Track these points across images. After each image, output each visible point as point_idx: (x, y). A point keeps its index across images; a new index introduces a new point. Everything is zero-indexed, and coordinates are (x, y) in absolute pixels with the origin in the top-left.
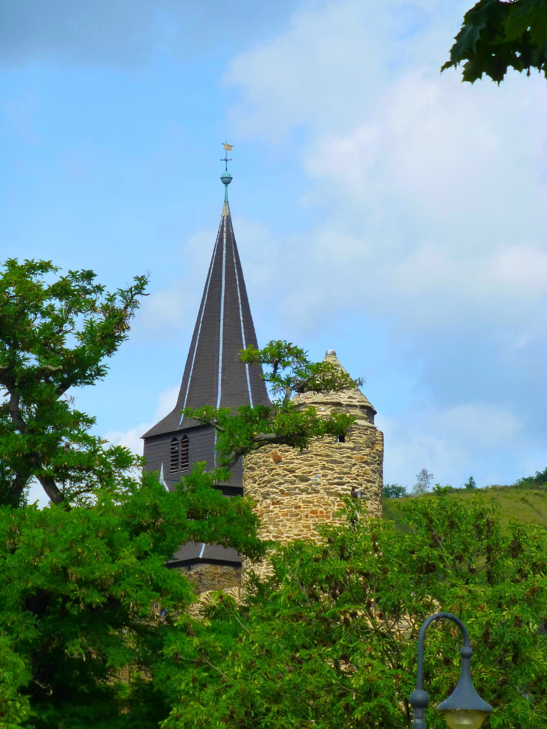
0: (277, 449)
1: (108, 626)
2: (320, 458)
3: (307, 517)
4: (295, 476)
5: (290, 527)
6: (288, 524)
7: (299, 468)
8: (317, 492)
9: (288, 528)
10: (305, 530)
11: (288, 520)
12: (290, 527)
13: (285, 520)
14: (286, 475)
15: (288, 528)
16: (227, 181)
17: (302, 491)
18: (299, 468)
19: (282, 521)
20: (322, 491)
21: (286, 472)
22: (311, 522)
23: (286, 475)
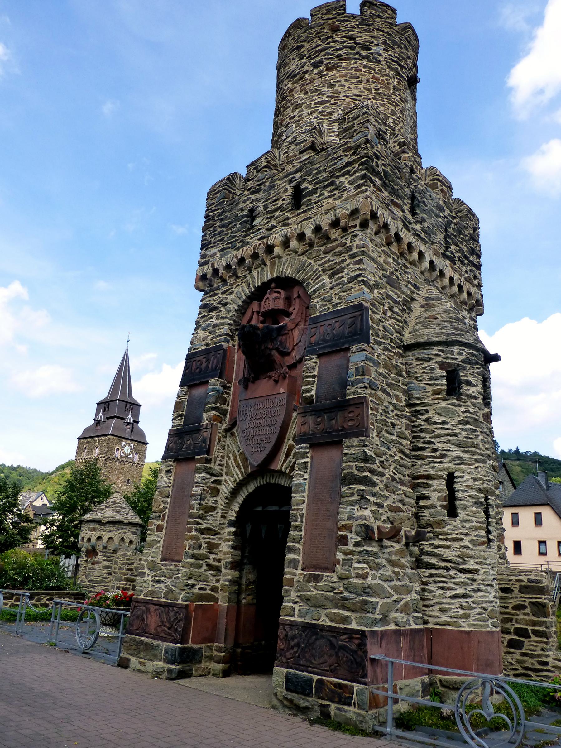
0: (334, 20)
1: (228, 665)
2: (382, 33)
3: (368, 81)
4: (355, 43)
5: (349, 87)
6: (347, 84)
7: (360, 37)
8: (379, 62)
9: (346, 88)
10: (366, 92)
11: (346, 81)
12: (349, 87)
13: (343, 81)
14: (344, 42)
15: (346, 88)
16: (128, 341)
17: (364, 57)
18: (360, 37)
19: (340, 81)
20: (383, 63)
21: (345, 39)
22: (373, 86)
23: (344, 42)
